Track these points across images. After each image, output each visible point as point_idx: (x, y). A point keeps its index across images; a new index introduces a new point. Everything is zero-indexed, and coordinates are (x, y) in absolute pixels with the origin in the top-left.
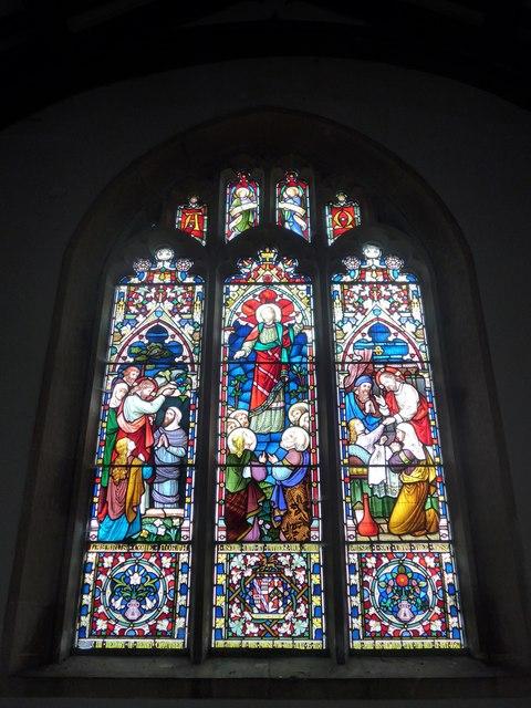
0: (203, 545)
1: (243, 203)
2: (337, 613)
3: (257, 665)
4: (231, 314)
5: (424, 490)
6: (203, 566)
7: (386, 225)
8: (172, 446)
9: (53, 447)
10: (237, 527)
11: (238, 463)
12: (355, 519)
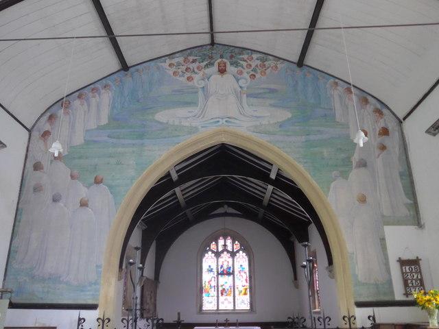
0: (218, 297)
1: (221, 242)
2: (234, 306)
3: (349, 247)
4: (220, 264)
5: (246, 289)
6: (218, 300)
7: (246, 248)
8: (214, 283)
9: (199, 286)
10: (222, 294)
11: (222, 286)
12: (237, 292)
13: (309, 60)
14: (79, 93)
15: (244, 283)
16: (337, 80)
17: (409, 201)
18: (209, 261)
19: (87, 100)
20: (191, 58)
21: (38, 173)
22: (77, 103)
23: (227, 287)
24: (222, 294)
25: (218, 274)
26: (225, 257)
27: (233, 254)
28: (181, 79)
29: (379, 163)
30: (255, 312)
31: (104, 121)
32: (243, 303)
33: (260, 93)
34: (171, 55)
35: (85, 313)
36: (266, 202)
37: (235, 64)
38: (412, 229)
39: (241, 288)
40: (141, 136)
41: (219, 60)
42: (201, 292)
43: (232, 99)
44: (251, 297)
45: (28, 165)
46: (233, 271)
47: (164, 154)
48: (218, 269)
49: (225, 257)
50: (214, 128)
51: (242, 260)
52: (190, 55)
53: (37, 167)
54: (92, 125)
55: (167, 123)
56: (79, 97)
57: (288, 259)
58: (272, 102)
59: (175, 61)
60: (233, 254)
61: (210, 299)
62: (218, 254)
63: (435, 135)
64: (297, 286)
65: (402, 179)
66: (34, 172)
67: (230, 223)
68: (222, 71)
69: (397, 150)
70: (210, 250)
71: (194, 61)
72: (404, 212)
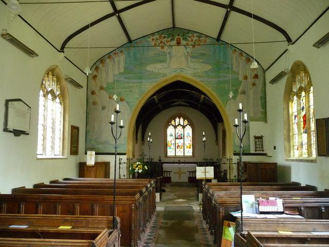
1: (177, 120)
4: (177, 132)
10: (177, 148)
13: (223, 38)
14: (109, 55)
15: (190, 142)
16: (236, 49)
17: (263, 111)
18: (170, 130)
19: (113, 59)
20: (163, 36)
21: (94, 96)
22: (108, 61)
23: (180, 144)
24: (177, 148)
25: (176, 138)
26: (180, 128)
27: (184, 127)
28: (158, 47)
29: (251, 92)
30: (195, 157)
31: (122, 70)
32: (189, 152)
33: (197, 56)
34: (153, 34)
35: (121, 157)
36: (201, 101)
37: (185, 39)
38: (262, 123)
39: (188, 145)
40: (140, 78)
41: (177, 37)
42: (223, 226)
43: (183, 58)
44: (193, 150)
45: (88, 92)
46: (184, 136)
47: (151, 87)
48: (175, 136)
49: (180, 128)
50: (173, 74)
51: (189, 130)
52: (162, 34)
53: (93, 93)
54: (116, 72)
55: (152, 71)
56: (109, 57)
57: (214, 132)
58: (203, 60)
59: (155, 37)
60: (184, 127)
61: (171, 150)
62: (175, 127)
63: (319, 47)
64: (217, 144)
65: (261, 100)
66: (92, 96)
67: (182, 110)
68: (179, 43)
69: (261, 86)
70: (171, 124)
71: (164, 37)
72: (260, 115)
